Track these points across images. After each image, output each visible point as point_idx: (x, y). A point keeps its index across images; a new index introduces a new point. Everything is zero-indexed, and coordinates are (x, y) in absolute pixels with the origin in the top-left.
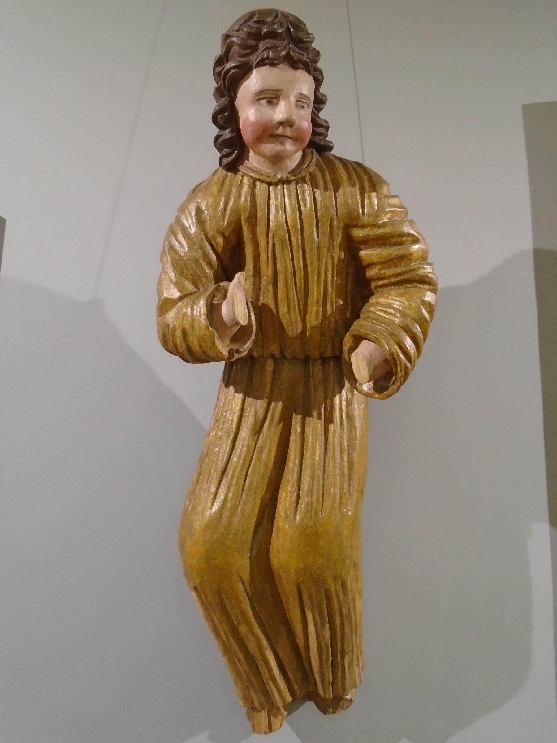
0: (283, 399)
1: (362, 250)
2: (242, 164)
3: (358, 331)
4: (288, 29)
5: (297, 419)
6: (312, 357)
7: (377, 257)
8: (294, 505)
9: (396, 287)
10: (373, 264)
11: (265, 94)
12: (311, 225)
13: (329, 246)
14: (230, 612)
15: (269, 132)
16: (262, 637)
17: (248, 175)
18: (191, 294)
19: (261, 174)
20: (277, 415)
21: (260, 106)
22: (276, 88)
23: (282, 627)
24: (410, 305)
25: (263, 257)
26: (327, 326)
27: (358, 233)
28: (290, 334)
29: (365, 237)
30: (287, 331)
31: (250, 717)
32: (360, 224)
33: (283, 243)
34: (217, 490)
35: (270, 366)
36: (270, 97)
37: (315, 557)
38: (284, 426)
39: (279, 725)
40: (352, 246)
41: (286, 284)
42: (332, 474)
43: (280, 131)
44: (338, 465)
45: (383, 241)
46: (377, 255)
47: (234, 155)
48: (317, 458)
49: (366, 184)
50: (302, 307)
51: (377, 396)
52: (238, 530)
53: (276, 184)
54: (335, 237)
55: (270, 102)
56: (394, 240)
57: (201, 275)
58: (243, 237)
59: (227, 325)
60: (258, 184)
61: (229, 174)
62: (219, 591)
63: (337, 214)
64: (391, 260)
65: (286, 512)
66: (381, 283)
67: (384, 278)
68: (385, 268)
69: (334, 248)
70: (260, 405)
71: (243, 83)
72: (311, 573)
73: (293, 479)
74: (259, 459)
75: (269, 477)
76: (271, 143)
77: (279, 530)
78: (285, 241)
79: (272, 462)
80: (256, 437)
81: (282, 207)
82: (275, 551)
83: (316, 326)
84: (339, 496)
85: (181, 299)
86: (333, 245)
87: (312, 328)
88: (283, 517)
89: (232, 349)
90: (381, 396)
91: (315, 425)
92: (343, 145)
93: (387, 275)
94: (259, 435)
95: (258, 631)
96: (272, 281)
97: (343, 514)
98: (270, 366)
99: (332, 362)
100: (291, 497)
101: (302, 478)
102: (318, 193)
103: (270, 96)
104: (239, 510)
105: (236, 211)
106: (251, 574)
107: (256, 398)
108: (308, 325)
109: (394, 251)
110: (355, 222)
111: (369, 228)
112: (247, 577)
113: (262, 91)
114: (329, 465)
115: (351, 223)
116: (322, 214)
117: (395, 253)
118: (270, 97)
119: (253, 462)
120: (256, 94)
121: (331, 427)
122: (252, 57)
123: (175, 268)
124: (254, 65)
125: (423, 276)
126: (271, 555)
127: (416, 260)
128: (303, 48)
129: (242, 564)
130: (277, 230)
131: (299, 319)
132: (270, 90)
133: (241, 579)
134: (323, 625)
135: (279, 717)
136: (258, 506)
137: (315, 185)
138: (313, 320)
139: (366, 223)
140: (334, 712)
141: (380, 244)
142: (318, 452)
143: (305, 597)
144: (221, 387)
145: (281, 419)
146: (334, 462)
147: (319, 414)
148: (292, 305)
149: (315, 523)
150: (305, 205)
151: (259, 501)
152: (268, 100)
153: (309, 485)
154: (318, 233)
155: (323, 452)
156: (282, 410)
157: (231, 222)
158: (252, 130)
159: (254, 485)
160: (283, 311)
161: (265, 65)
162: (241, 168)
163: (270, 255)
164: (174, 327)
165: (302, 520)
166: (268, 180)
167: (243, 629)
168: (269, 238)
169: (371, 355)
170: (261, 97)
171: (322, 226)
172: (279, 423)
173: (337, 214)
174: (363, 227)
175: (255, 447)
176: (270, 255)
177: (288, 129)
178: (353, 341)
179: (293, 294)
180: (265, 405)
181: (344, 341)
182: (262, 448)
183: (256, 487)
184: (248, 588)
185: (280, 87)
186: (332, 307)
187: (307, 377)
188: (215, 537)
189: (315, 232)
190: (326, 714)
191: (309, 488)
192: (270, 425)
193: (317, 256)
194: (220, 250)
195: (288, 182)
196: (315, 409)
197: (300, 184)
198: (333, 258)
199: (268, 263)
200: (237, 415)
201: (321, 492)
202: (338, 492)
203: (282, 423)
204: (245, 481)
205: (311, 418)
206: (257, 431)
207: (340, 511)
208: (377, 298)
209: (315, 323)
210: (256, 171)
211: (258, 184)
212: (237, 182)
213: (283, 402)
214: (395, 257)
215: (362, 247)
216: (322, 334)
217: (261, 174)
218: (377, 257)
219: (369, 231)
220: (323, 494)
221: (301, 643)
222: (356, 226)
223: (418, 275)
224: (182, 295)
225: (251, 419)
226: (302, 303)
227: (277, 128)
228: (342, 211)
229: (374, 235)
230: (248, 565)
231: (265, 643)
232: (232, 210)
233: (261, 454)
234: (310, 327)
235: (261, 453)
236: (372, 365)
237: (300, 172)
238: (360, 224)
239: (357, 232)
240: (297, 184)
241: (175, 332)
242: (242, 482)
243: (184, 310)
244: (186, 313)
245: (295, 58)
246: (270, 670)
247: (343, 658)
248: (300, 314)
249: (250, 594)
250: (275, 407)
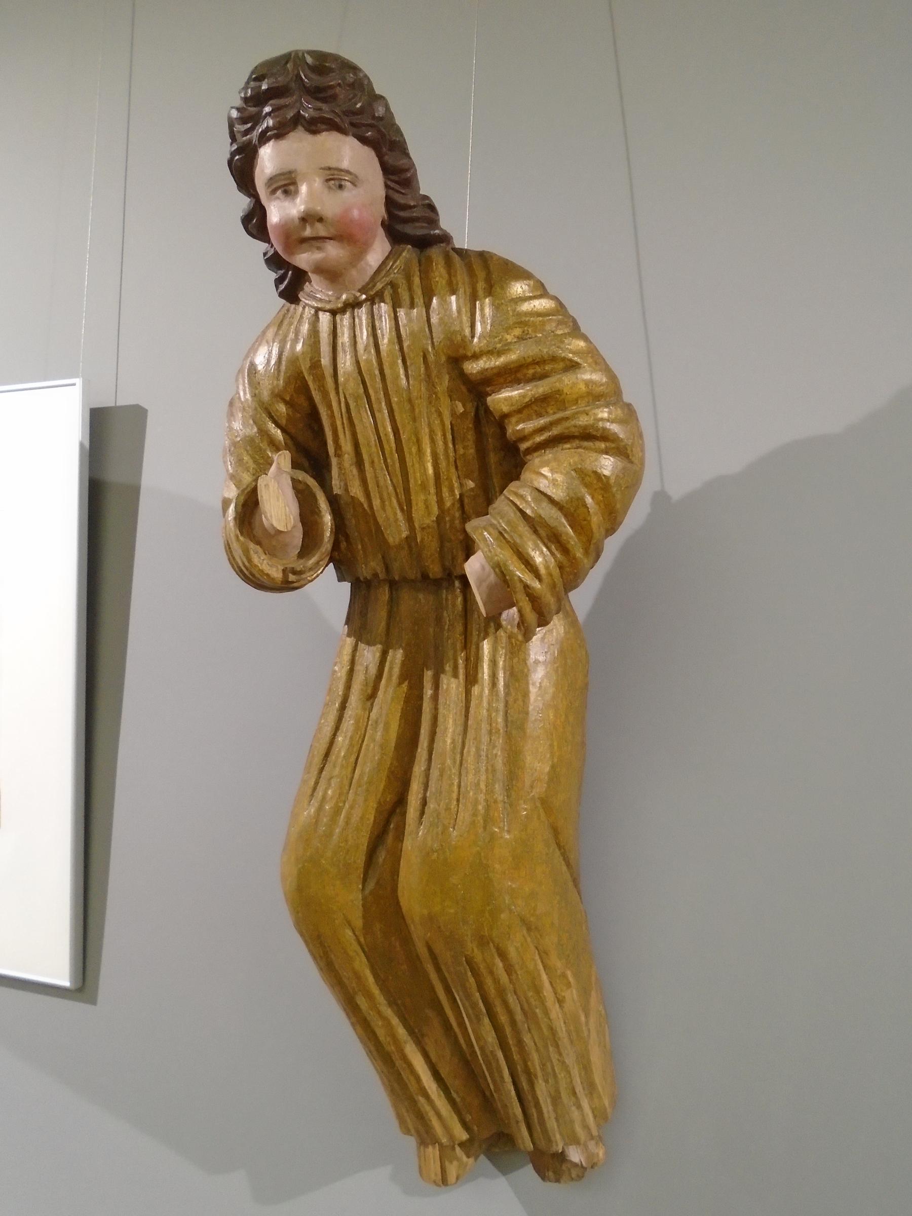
2: (302, 289)
4: (298, 76)
7: (506, 403)
12: (393, 364)
13: (430, 397)
16: (395, 1021)
20: (396, 671)
22: (287, 170)
23: (430, 1013)
25: (339, 423)
26: (448, 525)
27: (473, 368)
28: (391, 540)
31: (419, 1148)
32: (469, 354)
33: (357, 398)
34: (317, 783)
35: (384, 594)
38: (410, 687)
42: (472, 767)
43: (308, 232)
44: (483, 754)
45: (512, 375)
49: (481, 285)
52: (340, 847)
53: (343, 311)
55: (286, 192)
60: (321, 314)
62: (319, 937)
63: (433, 343)
69: (437, 398)
72: (439, 927)
75: (389, 768)
79: (393, 745)
80: (369, 704)
84: (484, 803)
86: (436, 393)
92: (463, 227)
93: (526, 432)
95: (388, 1012)
97: (492, 837)
102: (401, 313)
106: (364, 917)
107: (369, 643)
108: (417, 525)
109: (541, 388)
110: (461, 351)
112: (359, 923)
114: (469, 752)
116: (409, 346)
117: (530, 393)
119: (365, 743)
121: (476, 690)
125: (585, 427)
127: (576, 402)
128: (325, 98)
130: (347, 380)
131: (399, 515)
136: (373, 812)
141: (510, 382)
145: (403, 677)
146: (478, 750)
151: (373, 805)
155: (460, 729)
156: (403, 664)
157: (289, 378)
171: (412, 364)
172: (400, 684)
173: (433, 343)
174: (476, 357)
177: (319, 225)
180: (378, 655)
182: (376, 722)
184: (362, 940)
185: (292, 167)
188: (308, 854)
189: (403, 376)
190: (544, 1178)
192: (387, 686)
194: (283, 422)
198: (440, 414)
201: (455, 796)
202: (481, 797)
203: (406, 683)
204: (354, 772)
207: (485, 828)
211: (321, 314)
213: (404, 649)
214: (531, 400)
216: (442, 539)
218: (506, 403)
222: (466, 358)
226: (400, 490)
228: (438, 335)
229: (492, 369)
231: (401, 1032)
237: (374, 286)
238: (469, 354)
240: (373, 303)
246: (418, 1079)
247: (532, 1084)
248: (402, 510)
249: (366, 950)
250: (394, 657)
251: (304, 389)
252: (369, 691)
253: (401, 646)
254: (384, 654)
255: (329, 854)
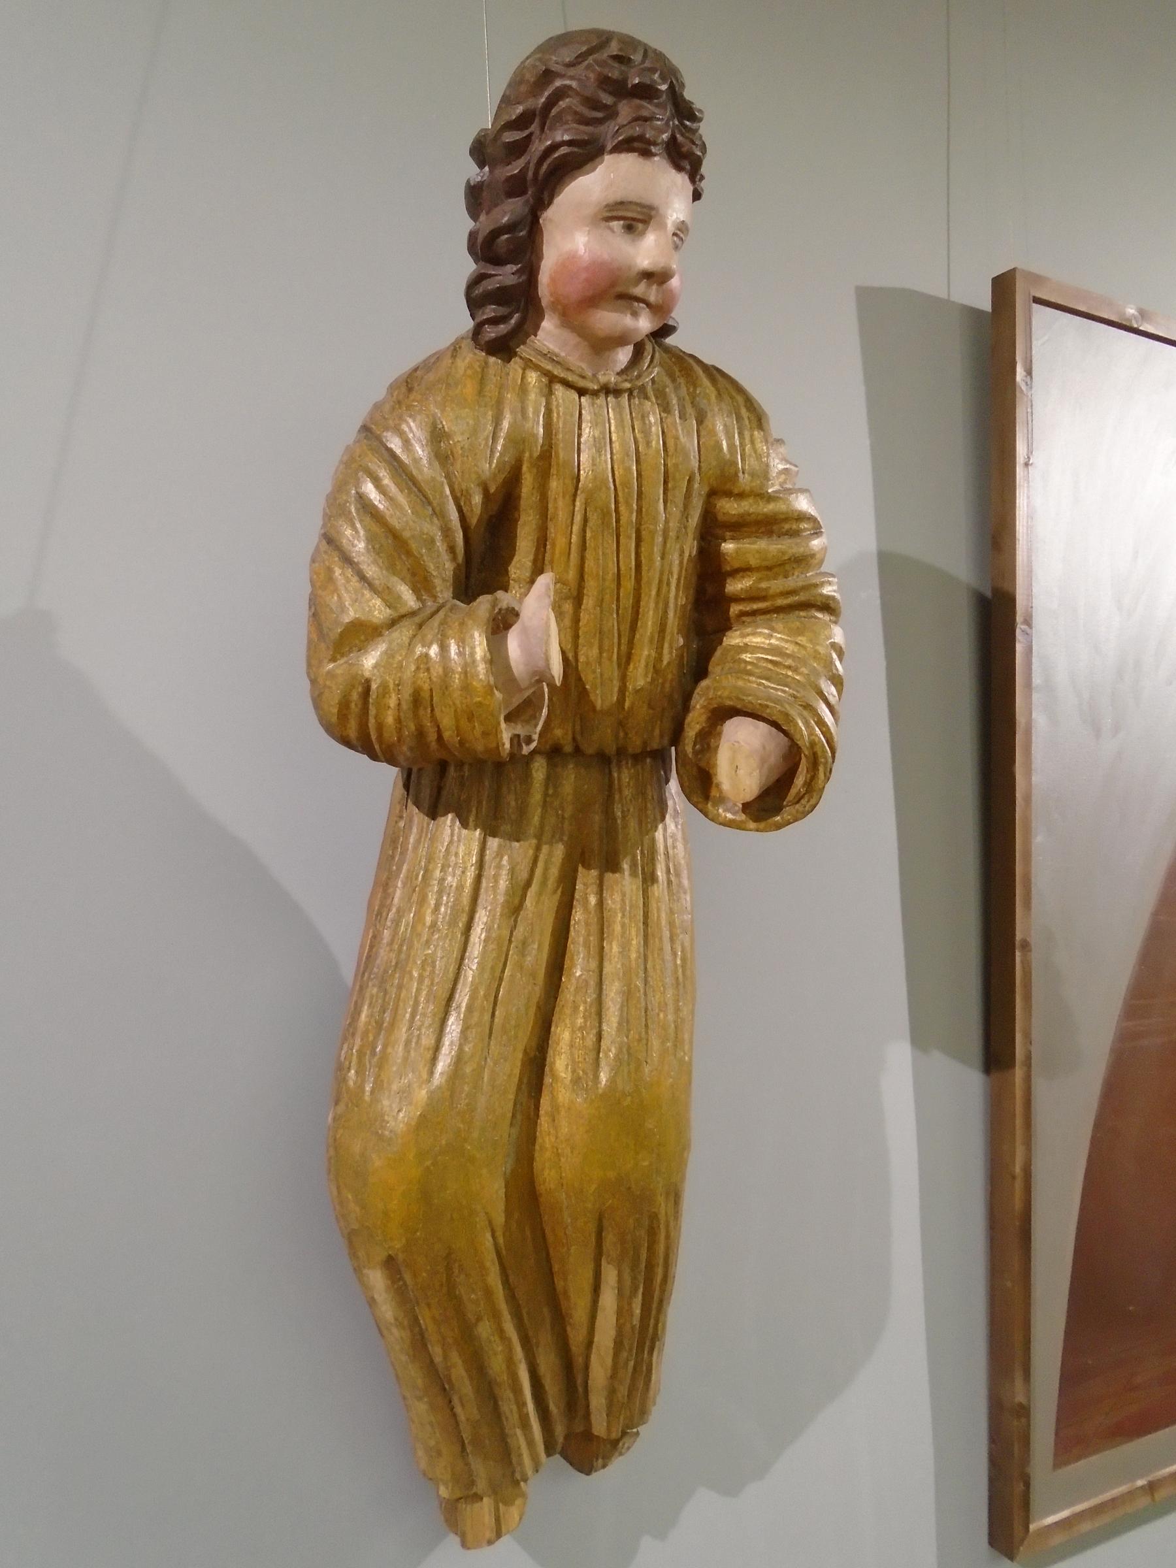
0: (565, 838)
1: (725, 541)
3: (738, 698)
5: (586, 879)
6: (630, 750)
7: (757, 556)
8: (593, 1055)
9: (782, 616)
10: (745, 570)
11: (627, 210)
14: (465, 1297)
15: (619, 289)
17: (537, 368)
18: (413, 614)
19: (568, 369)
21: (609, 232)
22: (648, 203)
24: (816, 651)
28: (599, 704)
29: (742, 516)
30: (592, 697)
35: (539, 771)
36: (633, 217)
37: (637, 1153)
39: (517, 1517)
40: (711, 530)
41: (600, 602)
46: (758, 552)
47: (513, 321)
48: (634, 956)
50: (624, 648)
51: (752, 825)
53: (595, 394)
54: (692, 513)
56: (787, 526)
57: (435, 573)
58: (519, 497)
59: (518, 685)
61: (492, 360)
64: (782, 564)
65: (574, 1071)
66: (755, 606)
67: (763, 598)
68: (768, 579)
70: (522, 850)
71: (576, 178)
73: (585, 1002)
74: (520, 967)
76: (616, 311)
77: (556, 1108)
78: (609, 513)
81: (601, 441)
82: (548, 1154)
83: (642, 689)
85: (393, 623)
86: (685, 528)
87: (637, 692)
88: (567, 1082)
89: (518, 736)
90: (762, 825)
91: (625, 885)
93: (771, 592)
94: (518, 914)
96: (575, 594)
98: (539, 771)
99: (648, 760)
100: (583, 1038)
101: (604, 997)
103: (634, 215)
104: (486, 1079)
105: (518, 441)
108: (630, 687)
111: (751, 500)
112: (500, 1219)
113: (622, 203)
115: (722, 485)
118: (633, 217)
120: (607, 206)
122: (602, 128)
123: (378, 554)
124: (609, 147)
126: (537, 1165)
129: (491, 1191)
132: (637, 204)
133: (490, 1222)
134: (635, 1289)
135: (518, 1502)
137: (666, 408)
138: (639, 677)
139: (748, 488)
140: (604, 1466)
142: (634, 942)
143: (610, 1238)
144: (395, 816)
147: (634, 865)
148: (606, 643)
149: (637, 1086)
150: (648, 444)
152: (628, 222)
153: (621, 1009)
154: (665, 502)
158: (587, 280)
159: (513, 1023)
160: (587, 657)
161: (631, 150)
162: (522, 350)
163: (574, 538)
164: (384, 687)
165: (612, 1081)
166: (582, 383)
167: (484, 1330)
168: (578, 503)
169: (764, 748)
170: (614, 214)
172: (555, 892)
174: (741, 496)
175: (510, 941)
176: (574, 538)
178: (709, 718)
179: (612, 622)
180: (531, 852)
181: (687, 721)
183: (517, 1026)
184: (501, 1240)
186: (671, 653)
187: (609, 791)
191: (621, 1016)
192: (540, 894)
193: (660, 547)
194: (474, 521)
195: (617, 392)
196: (625, 857)
197: (637, 401)
199: (569, 554)
200: (471, 874)
202: (671, 1017)
205: (617, 875)
206: (514, 909)
208: (743, 636)
209: (641, 683)
210: (558, 362)
211: (559, 390)
212: (514, 380)
215: (728, 534)
217: (568, 369)
218: (757, 556)
219: (751, 505)
220: (646, 1026)
221: (577, 1337)
222: (729, 494)
223: (822, 595)
224: (395, 615)
225: (503, 884)
226: (624, 640)
227: (637, 283)
230: (502, 1192)
232: (508, 438)
233: (523, 955)
234: (634, 689)
235: (522, 953)
236: (766, 766)
238: (736, 491)
239: (728, 506)
241: (384, 697)
242: (487, 1017)
243: (419, 650)
244: (427, 655)
245: (684, 149)
246: (521, 1405)
248: (619, 665)
250: (550, 854)
251: (512, 480)
252: (517, 901)
253: (561, 840)
254: (538, 849)
255: (475, 1135)
